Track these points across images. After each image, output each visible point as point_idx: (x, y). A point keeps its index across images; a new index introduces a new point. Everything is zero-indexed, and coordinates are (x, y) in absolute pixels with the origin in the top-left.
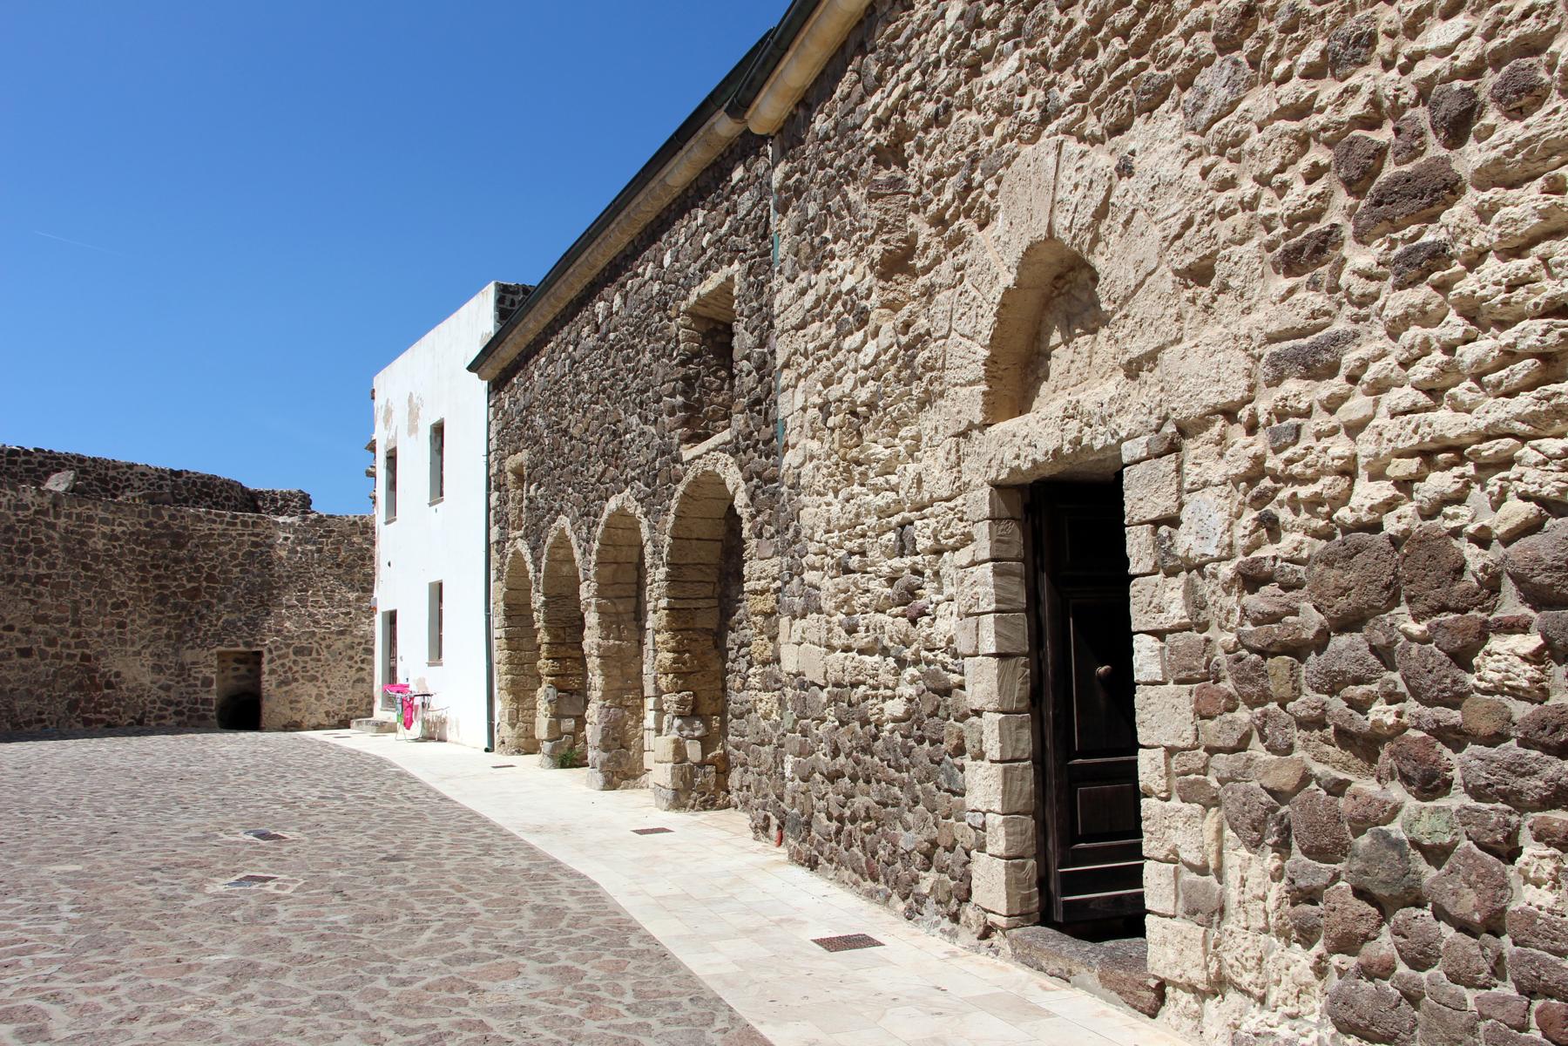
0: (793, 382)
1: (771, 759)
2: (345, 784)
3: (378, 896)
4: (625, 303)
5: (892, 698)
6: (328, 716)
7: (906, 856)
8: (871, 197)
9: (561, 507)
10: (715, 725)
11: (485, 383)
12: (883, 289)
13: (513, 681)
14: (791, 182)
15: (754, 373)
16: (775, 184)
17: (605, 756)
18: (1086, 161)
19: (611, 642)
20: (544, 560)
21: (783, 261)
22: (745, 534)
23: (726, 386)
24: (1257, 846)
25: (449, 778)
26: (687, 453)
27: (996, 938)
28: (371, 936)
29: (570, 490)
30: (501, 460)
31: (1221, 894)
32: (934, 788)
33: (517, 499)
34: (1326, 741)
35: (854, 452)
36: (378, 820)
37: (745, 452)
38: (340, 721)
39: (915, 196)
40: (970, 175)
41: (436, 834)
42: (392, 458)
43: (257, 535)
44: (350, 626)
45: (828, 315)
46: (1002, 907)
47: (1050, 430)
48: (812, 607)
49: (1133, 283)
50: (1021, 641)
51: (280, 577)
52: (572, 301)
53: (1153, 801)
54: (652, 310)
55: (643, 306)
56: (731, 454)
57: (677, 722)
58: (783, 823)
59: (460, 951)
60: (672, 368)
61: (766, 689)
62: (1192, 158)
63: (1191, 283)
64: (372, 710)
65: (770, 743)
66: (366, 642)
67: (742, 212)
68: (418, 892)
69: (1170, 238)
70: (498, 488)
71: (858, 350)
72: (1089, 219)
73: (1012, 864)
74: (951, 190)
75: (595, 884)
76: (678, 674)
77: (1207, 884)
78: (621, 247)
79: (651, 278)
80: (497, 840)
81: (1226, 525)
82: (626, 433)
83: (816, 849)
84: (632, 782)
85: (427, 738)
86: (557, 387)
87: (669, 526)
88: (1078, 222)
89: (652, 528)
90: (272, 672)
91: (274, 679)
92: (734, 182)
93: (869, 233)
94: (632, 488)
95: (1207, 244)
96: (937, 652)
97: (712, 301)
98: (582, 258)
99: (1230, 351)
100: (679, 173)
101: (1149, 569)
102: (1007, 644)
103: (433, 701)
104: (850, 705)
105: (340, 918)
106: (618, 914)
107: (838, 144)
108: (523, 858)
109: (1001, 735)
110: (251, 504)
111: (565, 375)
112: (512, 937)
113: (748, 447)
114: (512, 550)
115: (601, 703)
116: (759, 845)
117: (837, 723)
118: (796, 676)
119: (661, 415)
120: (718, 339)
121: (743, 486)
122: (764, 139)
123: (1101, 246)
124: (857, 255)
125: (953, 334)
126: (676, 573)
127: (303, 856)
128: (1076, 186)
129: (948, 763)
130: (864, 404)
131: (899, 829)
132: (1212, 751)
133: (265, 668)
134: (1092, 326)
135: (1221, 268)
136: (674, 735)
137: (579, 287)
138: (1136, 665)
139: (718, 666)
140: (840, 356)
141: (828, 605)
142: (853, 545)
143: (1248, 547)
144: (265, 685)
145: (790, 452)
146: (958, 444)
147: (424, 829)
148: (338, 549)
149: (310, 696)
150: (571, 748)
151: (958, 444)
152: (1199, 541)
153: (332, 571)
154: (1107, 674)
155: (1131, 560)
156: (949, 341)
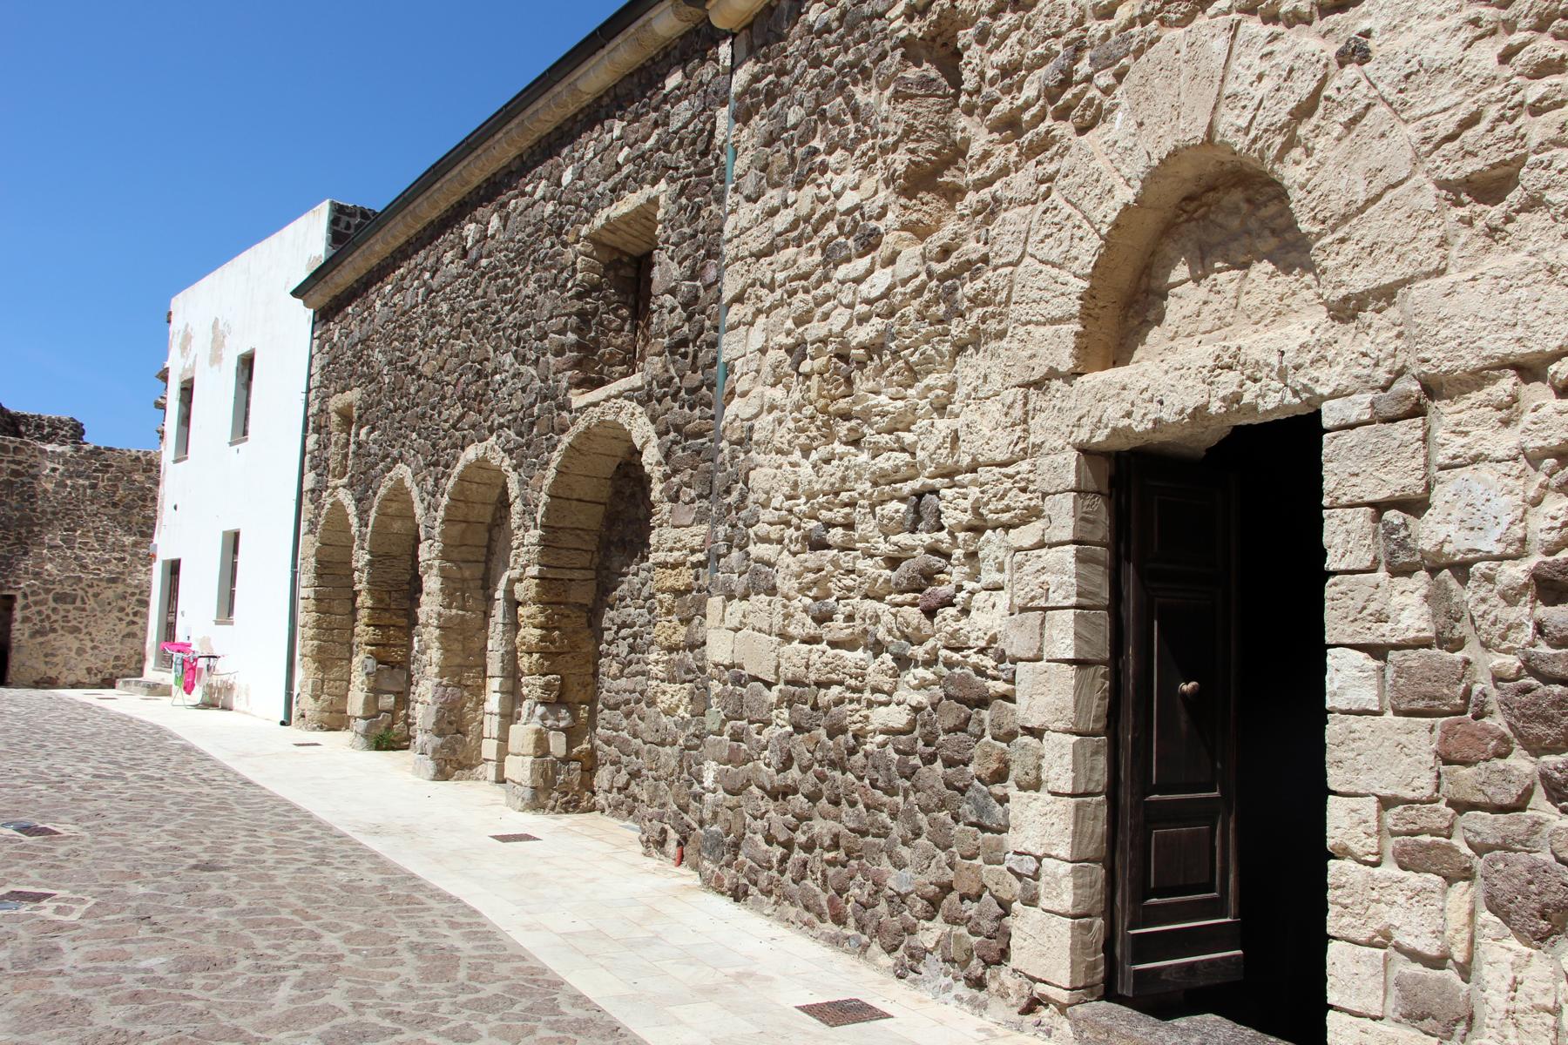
0: (749, 318)
1: (673, 763)
2: (120, 759)
3: (200, 925)
4: (505, 226)
5: (887, 704)
6: (89, 673)
7: (897, 900)
8: (898, 97)
9: (401, 453)
10: (583, 714)
11: (310, 312)
12: (905, 208)
13: (319, 648)
14: (761, 85)
15: (679, 310)
16: (736, 87)
17: (438, 741)
18: (1277, 46)
19: (454, 611)
20: (373, 514)
21: (740, 177)
22: (655, 495)
23: (627, 327)
24: (1542, 940)
25: (246, 755)
26: (578, 399)
27: (1044, 1013)
28: (207, 995)
29: (414, 436)
30: (324, 399)
31: (1468, 997)
32: (949, 820)
33: (340, 443)
35: (842, 404)
36: (174, 809)
37: (659, 401)
38: (104, 680)
39: (970, 94)
40: (1071, 67)
41: (252, 832)
42: (187, 390)
43: (19, 463)
44: (123, 573)
45: (810, 239)
46: (1063, 976)
47: (1190, 383)
48: (761, 583)
49: (1361, 198)
50: (1101, 648)
51: (44, 512)
52: (433, 222)
53: (1348, 864)
54: (542, 234)
55: (529, 230)
56: (640, 403)
57: (540, 710)
58: (685, 839)
59: (339, 1021)
60: (564, 301)
61: (672, 680)
62: (1481, 37)
63: (1465, 198)
64: (142, 669)
65: (674, 743)
66: (141, 593)
67: (675, 124)
68: (253, 918)
69: (1436, 139)
70: (318, 430)
71: (858, 281)
72: (1284, 117)
73: (1080, 925)
74: (1036, 85)
75: (475, 912)
76: (545, 654)
77: (1444, 982)
78: (504, 162)
79: (543, 198)
80: (330, 842)
81: (1519, 512)
82: (495, 372)
83: (745, 876)
84: (466, 772)
85: (208, 704)
86: (404, 319)
87: (548, 482)
88: (1263, 119)
89: (523, 483)
90: (26, 620)
91: (27, 629)
92: (668, 89)
93: (890, 139)
94: (499, 437)
95: (1507, 147)
96: (966, 652)
97: (624, 227)
98: (455, 172)
99: (1541, 286)
100: (595, 77)
101: (1367, 564)
102: (1086, 648)
103: (220, 665)
104: (815, 707)
105: (156, 962)
106: (523, 959)
107: (842, 37)
108: (371, 870)
109: (1075, 762)
110: (12, 429)
111: (416, 305)
112: (401, 996)
113: (665, 395)
114: (331, 500)
115: (438, 680)
116: (652, 863)
117: (789, 729)
118: (727, 668)
119: (544, 355)
120: (622, 272)
121: (655, 440)
122: (725, 35)
123: (1296, 153)
124: (864, 168)
125: (1027, 260)
126: (551, 537)
127: (87, 861)
128: (1260, 77)
129: (979, 791)
130: (861, 346)
131: (886, 864)
132: (1461, 807)
133: (18, 614)
134: (1242, 259)
135: (1529, 178)
136: (536, 724)
137: (444, 206)
138: (1329, 687)
139: (590, 648)
140: (828, 288)
141: (786, 585)
142: (838, 514)
143: (1557, 544)
144: (15, 634)
145: (736, 401)
146: (1026, 397)
147: (235, 824)
148: (115, 486)
149: (70, 649)
150: (389, 728)
151: (1026, 397)
152: (1464, 533)
153: (107, 511)
155: (1330, 552)
156: (1021, 268)
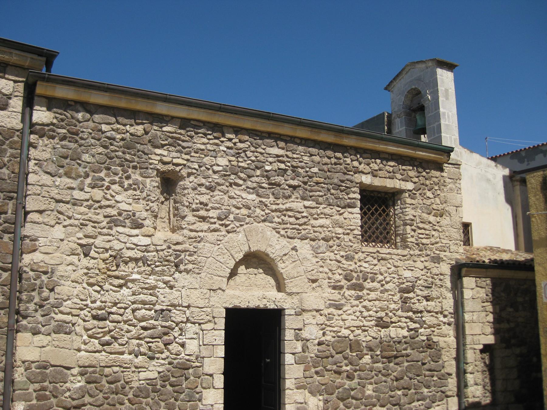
34: (332, 374)
154: (268, 362)
